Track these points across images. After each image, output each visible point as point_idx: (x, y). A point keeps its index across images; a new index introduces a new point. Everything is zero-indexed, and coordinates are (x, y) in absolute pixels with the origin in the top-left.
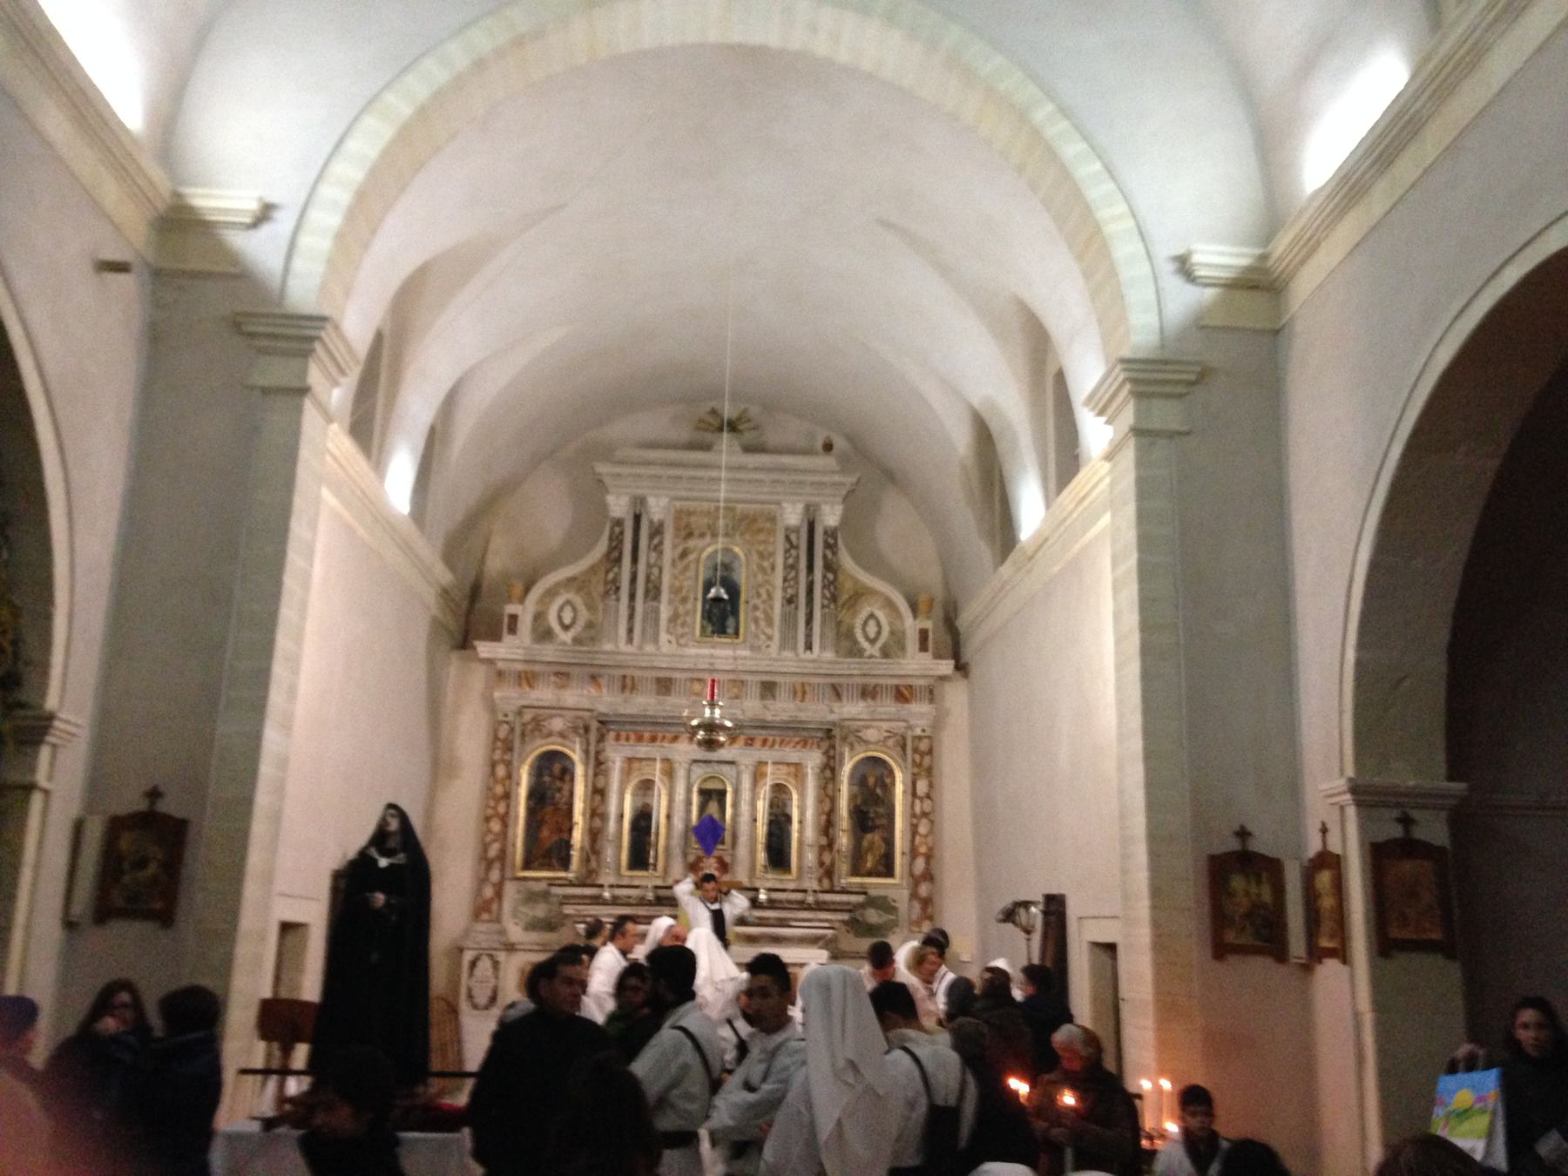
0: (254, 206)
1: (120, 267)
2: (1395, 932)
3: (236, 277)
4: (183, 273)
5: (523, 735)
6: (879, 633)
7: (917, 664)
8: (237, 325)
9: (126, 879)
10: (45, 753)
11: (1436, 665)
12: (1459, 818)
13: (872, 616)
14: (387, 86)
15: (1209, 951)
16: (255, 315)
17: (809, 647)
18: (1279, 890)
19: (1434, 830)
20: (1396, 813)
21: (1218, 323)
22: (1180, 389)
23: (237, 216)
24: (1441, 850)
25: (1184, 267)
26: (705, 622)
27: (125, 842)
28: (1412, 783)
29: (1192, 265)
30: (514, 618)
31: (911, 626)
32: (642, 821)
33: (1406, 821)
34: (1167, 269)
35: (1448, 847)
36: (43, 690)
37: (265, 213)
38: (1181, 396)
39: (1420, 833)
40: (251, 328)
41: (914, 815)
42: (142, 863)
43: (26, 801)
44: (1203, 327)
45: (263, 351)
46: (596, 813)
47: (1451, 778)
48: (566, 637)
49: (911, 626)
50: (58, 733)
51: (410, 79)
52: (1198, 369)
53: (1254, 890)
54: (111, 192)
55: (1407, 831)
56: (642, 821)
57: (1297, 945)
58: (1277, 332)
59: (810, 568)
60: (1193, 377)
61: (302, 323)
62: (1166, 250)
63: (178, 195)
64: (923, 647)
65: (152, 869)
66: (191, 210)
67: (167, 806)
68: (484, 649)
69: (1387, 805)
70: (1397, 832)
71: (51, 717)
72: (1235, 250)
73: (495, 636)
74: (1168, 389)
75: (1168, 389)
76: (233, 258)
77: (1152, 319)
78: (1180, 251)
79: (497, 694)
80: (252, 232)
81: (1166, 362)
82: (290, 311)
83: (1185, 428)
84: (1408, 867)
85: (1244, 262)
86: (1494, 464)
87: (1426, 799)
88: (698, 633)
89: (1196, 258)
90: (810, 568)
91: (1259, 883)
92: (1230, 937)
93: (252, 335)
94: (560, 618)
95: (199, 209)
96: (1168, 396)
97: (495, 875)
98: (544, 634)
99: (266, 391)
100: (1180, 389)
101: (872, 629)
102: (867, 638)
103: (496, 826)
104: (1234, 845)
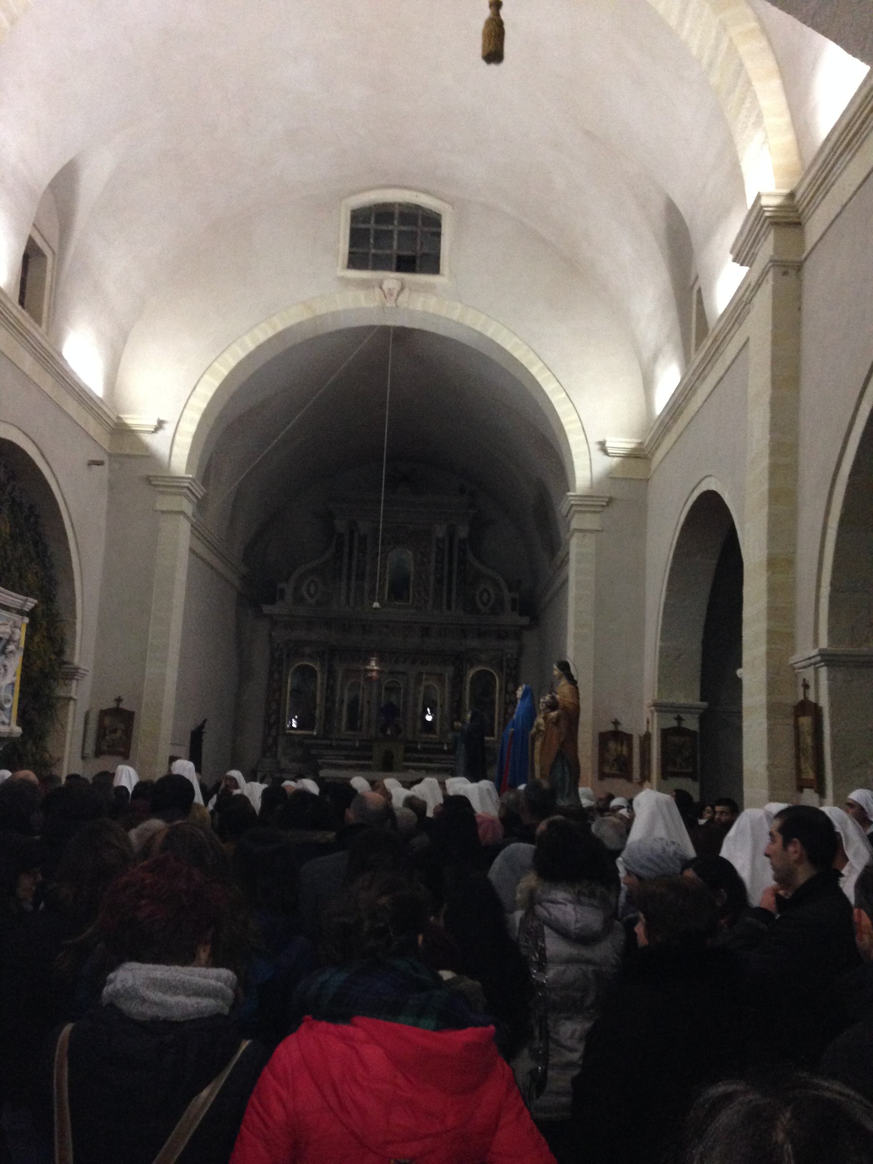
0: (155, 423)
1: (99, 463)
2: (670, 769)
3: (148, 457)
4: (121, 455)
5: (288, 656)
6: (489, 600)
7: (511, 618)
8: (148, 480)
9: (107, 737)
10: (74, 683)
11: (696, 647)
12: (704, 718)
13: (486, 590)
14: (214, 361)
15: (596, 775)
16: (157, 477)
17: (449, 608)
18: (630, 749)
19: (692, 723)
20: (675, 715)
21: (618, 476)
22: (599, 509)
23: (146, 427)
24: (694, 732)
25: (603, 447)
26: (107, 983)
27: (107, 721)
28: (682, 702)
29: (606, 447)
30: (282, 591)
31: (507, 596)
32: (354, 705)
33: (679, 719)
34: (595, 448)
35: (698, 731)
36: (72, 655)
37: (160, 425)
38: (599, 512)
39: (684, 725)
40: (153, 483)
41: (506, 703)
42: (114, 731)
43: (68, 704)
44: (611, 478)
45: (162, 493)
46: (330, 698)
47: (702, 700)
48: (312, 601)
49: (507, 596)
50: (80, 675)
51: (226, 355)
52: (607, 500)
53: (619, 748)
54: (93, 428)
55: (679, 723)
56: (354, 705)
57: (636, 774)
58: (648, 480)
59: (450, 563)
60: (604, 504)
61: (180, 480)
62: (594, 439)
63: (119, 418)
64: (513, 609)
65: (119, 734)
66: (126, 425)
67: (124, 706)
68: (266, 609)
69: (671, 712)
70: (674, 723)
71: (77, 668)
72: (628, 440)
73: (272, 602)
74: (592, 509)
75: (592, 509)
76: (145, 447)
77: (587, 474)
78: (601, 440)
79: (273, 634)
80: (154, 434)
81: (592, 497)
82: (173, 475)
83: (600, 529)
84: (676, 739)
85: (632, 446)
86: (715, 562)
87: (688, 709)
88: (386, 598)
89: (607, 445)
90: (450, 563)
91: (621, 746)
92: (607, 770)
93: (155, 486)
94: (308, 591)
95: (128, 424)
96: (590, 512)
97: (273, 732)
98: (299, 600)
99: (163, 512)
100: (599, 509)
101: (485, 597)
102: (482, 603)
103: (274, 706)
104: (611, 727)
